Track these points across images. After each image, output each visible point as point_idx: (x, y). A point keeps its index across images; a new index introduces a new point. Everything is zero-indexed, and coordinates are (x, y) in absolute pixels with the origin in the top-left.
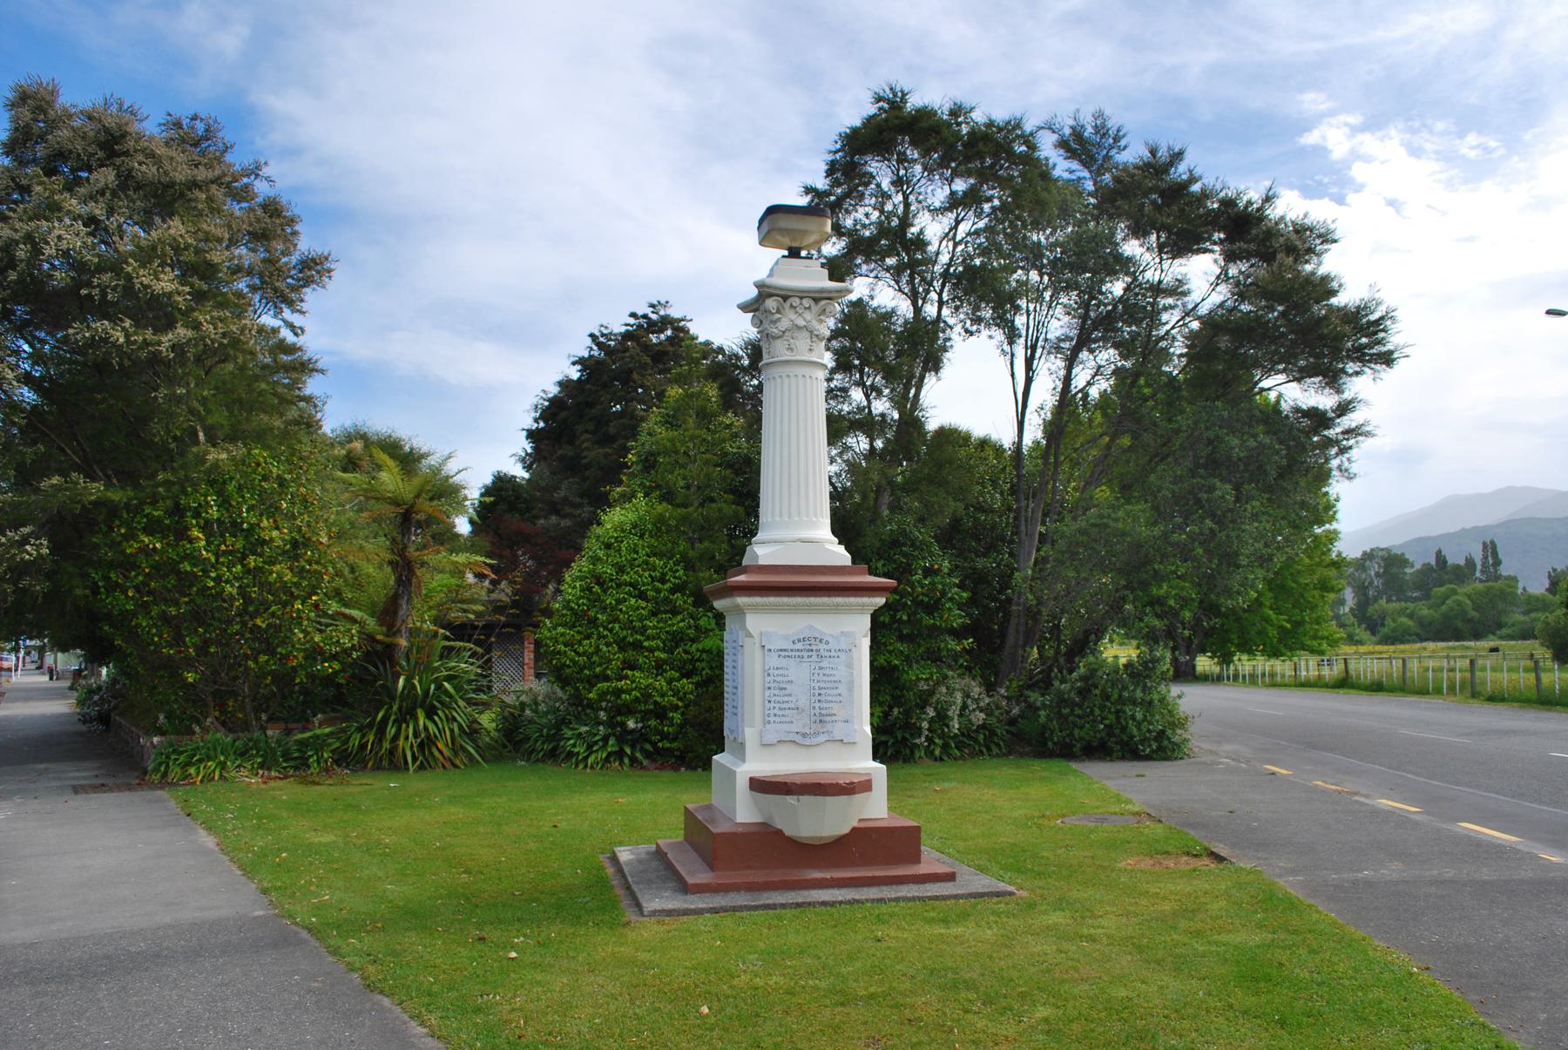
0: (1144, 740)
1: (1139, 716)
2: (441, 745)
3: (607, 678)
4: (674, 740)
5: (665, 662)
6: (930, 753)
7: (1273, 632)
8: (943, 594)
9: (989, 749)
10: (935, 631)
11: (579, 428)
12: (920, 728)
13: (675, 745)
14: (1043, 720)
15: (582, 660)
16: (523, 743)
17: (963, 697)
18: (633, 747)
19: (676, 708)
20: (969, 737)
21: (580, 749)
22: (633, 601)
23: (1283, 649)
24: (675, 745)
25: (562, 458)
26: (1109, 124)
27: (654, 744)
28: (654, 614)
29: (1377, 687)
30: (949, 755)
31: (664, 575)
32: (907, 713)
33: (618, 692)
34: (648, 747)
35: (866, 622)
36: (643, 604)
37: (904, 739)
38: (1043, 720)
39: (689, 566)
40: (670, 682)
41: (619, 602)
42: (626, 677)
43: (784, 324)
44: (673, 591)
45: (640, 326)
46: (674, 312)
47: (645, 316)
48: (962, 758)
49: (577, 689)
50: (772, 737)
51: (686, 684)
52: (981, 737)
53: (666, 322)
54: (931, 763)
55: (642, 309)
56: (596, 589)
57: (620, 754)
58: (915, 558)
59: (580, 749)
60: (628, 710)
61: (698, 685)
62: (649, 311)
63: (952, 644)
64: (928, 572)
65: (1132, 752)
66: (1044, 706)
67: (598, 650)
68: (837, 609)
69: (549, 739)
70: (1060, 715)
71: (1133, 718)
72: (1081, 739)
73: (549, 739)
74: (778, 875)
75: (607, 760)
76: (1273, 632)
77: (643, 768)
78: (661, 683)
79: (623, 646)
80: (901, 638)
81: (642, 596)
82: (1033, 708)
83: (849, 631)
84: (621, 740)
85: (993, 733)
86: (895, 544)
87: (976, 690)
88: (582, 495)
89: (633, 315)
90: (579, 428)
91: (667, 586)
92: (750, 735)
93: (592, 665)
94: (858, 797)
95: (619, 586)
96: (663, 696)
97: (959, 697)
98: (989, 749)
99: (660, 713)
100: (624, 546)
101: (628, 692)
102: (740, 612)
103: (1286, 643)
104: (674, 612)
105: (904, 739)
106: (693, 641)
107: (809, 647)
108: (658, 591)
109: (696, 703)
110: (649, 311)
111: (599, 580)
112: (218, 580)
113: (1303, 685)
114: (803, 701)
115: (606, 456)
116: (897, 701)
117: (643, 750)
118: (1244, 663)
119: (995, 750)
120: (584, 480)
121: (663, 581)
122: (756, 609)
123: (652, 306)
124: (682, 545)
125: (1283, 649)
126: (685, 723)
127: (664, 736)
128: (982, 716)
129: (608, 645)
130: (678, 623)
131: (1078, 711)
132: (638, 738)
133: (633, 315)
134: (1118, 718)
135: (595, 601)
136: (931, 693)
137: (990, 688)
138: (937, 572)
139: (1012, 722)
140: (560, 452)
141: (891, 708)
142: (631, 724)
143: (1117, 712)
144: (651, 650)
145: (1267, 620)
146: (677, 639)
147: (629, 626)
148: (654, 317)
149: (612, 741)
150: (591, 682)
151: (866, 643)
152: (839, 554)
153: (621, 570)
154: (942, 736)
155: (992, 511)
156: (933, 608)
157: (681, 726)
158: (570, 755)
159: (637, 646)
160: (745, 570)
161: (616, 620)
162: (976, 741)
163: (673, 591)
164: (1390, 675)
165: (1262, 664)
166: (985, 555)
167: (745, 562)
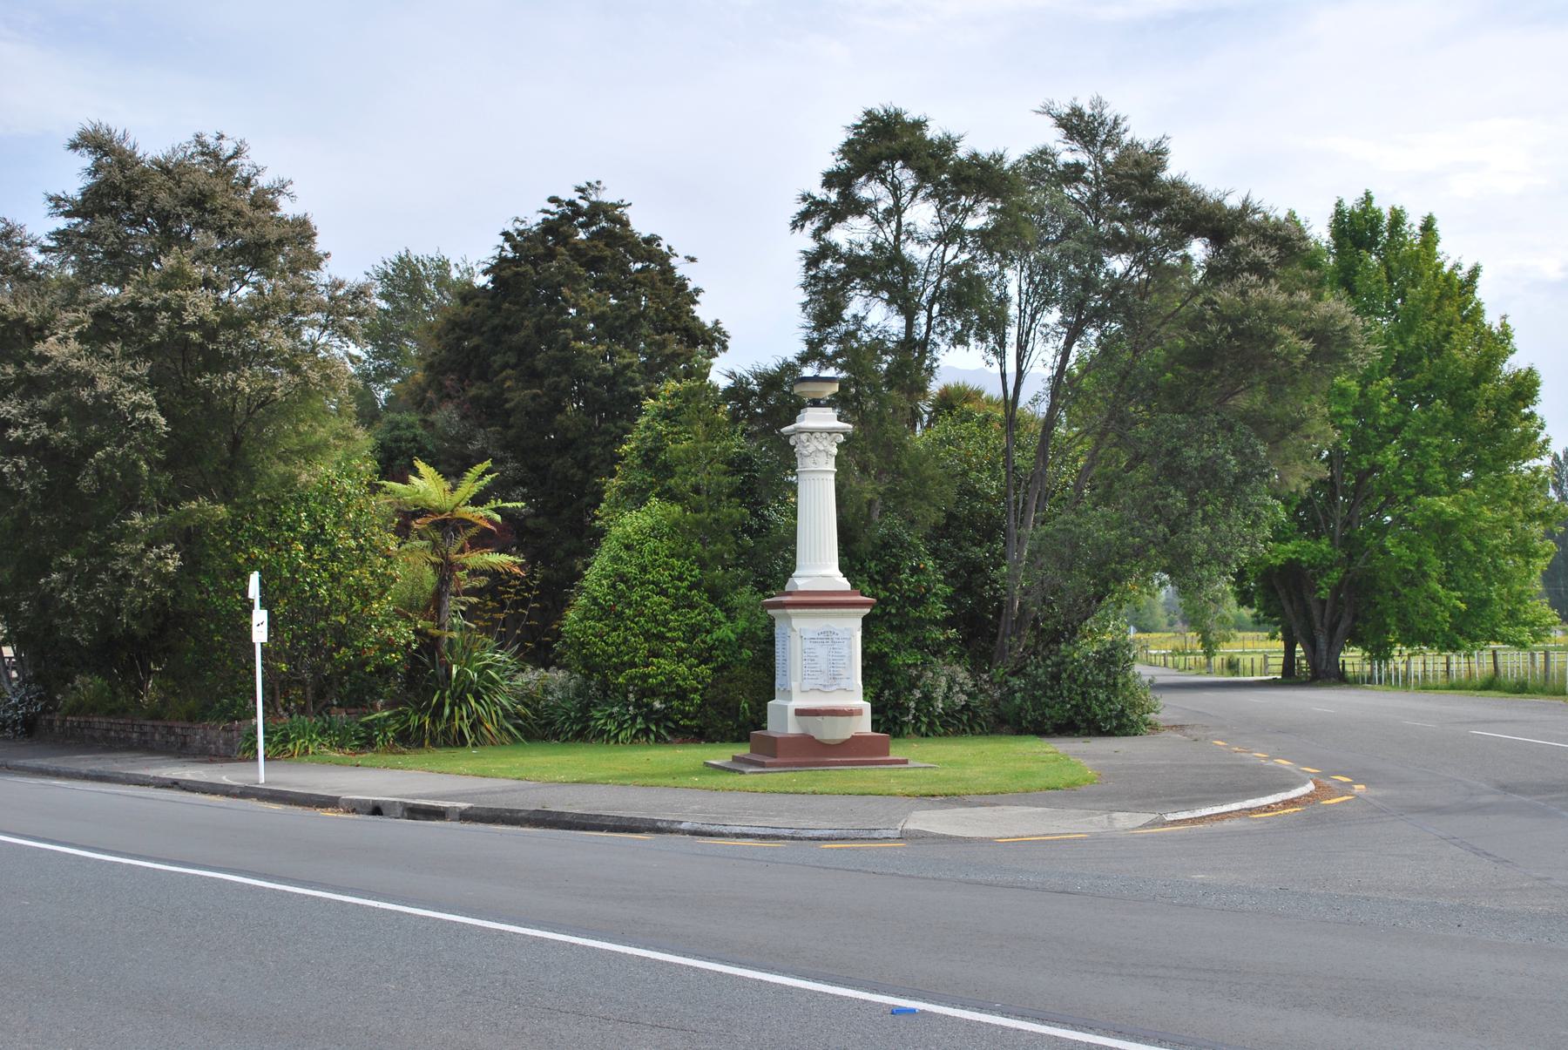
0: (1106, 719)
1: (1102, 697)
2: (489, 725)
3: (633, 665)
4: (692, 719)
5: (685, 650)
6: (917, 731)
7: (1443, 616)
8: (928, 590)
9: (972, 729)
10: (920, 623)
11: (497, 360)
12: (908, 708)
13: (694, 723)
14: (1018, 701)
15: (611, 650)
16: (539, 726)
17: (949, 680)
18: (657, 725)
19: (695, 690)
20: (953, 716)
21: (611, 727)
22: (656, 598)
23: (1460, 640)
24: (694, 723)
25: (475, 400)
26: (1106, 112)
27: (676, 723)
28: (674, 609)
29: (1521, 688)
30: (935, 733)
31: (681, 574)
32: (897, 695)
33: (644, 677)
34: (670, 724)
35: (859, 622)
36: (664, 599)
37: (895, 717)
38: (1018, 701)
39: (703, 566)
40: (690, 668)
41: (643, 598)
42: (652, 664)
43: (811, 449)
44: (690, 588)
45: (563, 216)
46: (607, 197)
47: (571, 203)
48: (946, 734)
49: (605, 676)
50: (806, 688)
51: (704, 670)
52: (965, 718)
53: (598, 210)
54: (918, 738)
55: (569, 194)
56: (621, 586)
57: (647, 732)
58: (903, 559)
59: (611, 727)
60: (654, 693)
61: (714, 670)
62: (575, 196)
63: (939, 635)
64: (915, 570)
65: (1095, 729)
66: (1021, 690)
67: (626, 640)
68: (842, 615)
69: (576, 721)
70: (1034, 697)
71: (1096, 698)
72: (1052, 717)
73: (576, 721)
74: (812, 760)
75: (635, 737)
76: (1443, 616)
77: (666, 742)
78: (683, 669)
79: (648, 636)
80: (892, 629)
81: (663, 592)
82: (1012, 692)
83: (850, 628)
84: (646, 718)
85: (976, 715)
86: (886, 545)
87: (962, 675)
88: (505, 448)
89: (553, 200)
90: (497, 360)
91: (686, 583)
92: (794, 685)
93: (619, 653)
94: (855, 718)
95: (642, 584)
96: (684, 680)
97: (943, 682)
98: (972, 729)
99: (682, 694)
100: (646, 548)
101: (655, 676)
102: (789, 617)
103: (1459, 633)
104: (692, 606)
105: (895, 717)
106: (708, 632)
107: (827, 637)
108: (678, 588)
109: (713, 686)
110: (575, 196)
111: (622, 578)
112: (312, 585)
113: (1452, 687)
114: (824, 667)
115: (534, 397)
116: (888, 684)
117: (666, 727)
118: (1402, 659)
119: (978, 729)
120: (507, 427)
121: (680, 578)
122: (797, 615)
123: (580, 190)
124: (698, 547)
125: (1460, 640)
126: (704, 702)
127: (686, 715)
128: (964, 697)
129: (635, 636)
130: (695, 617)
131: (1050, 693)
132: (661, 718)
133: (553, 200)
134: (1084, 699)
135: (620, 596)
136: (919, 677)
137: (974, 671)
138: (923, 571)
139: (995, 704)
140: (473, 392)
141: (882, 690)
142: (657, 705)
143: (1083, 693)
144: (673, 640)
145: (1434, 598)
146: (694, 631)
147: (653, 618)
148: (584, 204)
149: (639, 720)
150: (619, 668)
151: (859, 634)
152: (845, 584)
153: (644, 569)
154: (928, 714)
155: (987, 498)
156: (919, 601)
157: (700, 706)
158: (602, 732)
159: (661, 637)
160: (790, 593)
161: (642, 614)
162: (960, 721)
163: (690, 588)
164: (1533, 675)
165: (1427, 661)
166: (980, 545)
167: (787, 588)
